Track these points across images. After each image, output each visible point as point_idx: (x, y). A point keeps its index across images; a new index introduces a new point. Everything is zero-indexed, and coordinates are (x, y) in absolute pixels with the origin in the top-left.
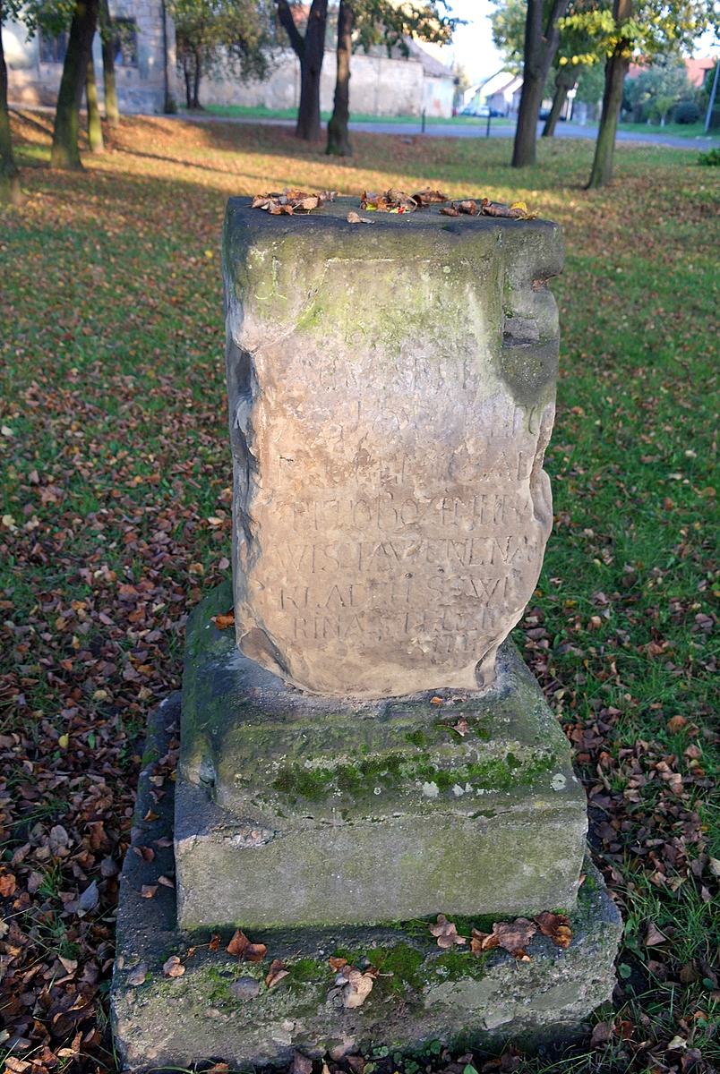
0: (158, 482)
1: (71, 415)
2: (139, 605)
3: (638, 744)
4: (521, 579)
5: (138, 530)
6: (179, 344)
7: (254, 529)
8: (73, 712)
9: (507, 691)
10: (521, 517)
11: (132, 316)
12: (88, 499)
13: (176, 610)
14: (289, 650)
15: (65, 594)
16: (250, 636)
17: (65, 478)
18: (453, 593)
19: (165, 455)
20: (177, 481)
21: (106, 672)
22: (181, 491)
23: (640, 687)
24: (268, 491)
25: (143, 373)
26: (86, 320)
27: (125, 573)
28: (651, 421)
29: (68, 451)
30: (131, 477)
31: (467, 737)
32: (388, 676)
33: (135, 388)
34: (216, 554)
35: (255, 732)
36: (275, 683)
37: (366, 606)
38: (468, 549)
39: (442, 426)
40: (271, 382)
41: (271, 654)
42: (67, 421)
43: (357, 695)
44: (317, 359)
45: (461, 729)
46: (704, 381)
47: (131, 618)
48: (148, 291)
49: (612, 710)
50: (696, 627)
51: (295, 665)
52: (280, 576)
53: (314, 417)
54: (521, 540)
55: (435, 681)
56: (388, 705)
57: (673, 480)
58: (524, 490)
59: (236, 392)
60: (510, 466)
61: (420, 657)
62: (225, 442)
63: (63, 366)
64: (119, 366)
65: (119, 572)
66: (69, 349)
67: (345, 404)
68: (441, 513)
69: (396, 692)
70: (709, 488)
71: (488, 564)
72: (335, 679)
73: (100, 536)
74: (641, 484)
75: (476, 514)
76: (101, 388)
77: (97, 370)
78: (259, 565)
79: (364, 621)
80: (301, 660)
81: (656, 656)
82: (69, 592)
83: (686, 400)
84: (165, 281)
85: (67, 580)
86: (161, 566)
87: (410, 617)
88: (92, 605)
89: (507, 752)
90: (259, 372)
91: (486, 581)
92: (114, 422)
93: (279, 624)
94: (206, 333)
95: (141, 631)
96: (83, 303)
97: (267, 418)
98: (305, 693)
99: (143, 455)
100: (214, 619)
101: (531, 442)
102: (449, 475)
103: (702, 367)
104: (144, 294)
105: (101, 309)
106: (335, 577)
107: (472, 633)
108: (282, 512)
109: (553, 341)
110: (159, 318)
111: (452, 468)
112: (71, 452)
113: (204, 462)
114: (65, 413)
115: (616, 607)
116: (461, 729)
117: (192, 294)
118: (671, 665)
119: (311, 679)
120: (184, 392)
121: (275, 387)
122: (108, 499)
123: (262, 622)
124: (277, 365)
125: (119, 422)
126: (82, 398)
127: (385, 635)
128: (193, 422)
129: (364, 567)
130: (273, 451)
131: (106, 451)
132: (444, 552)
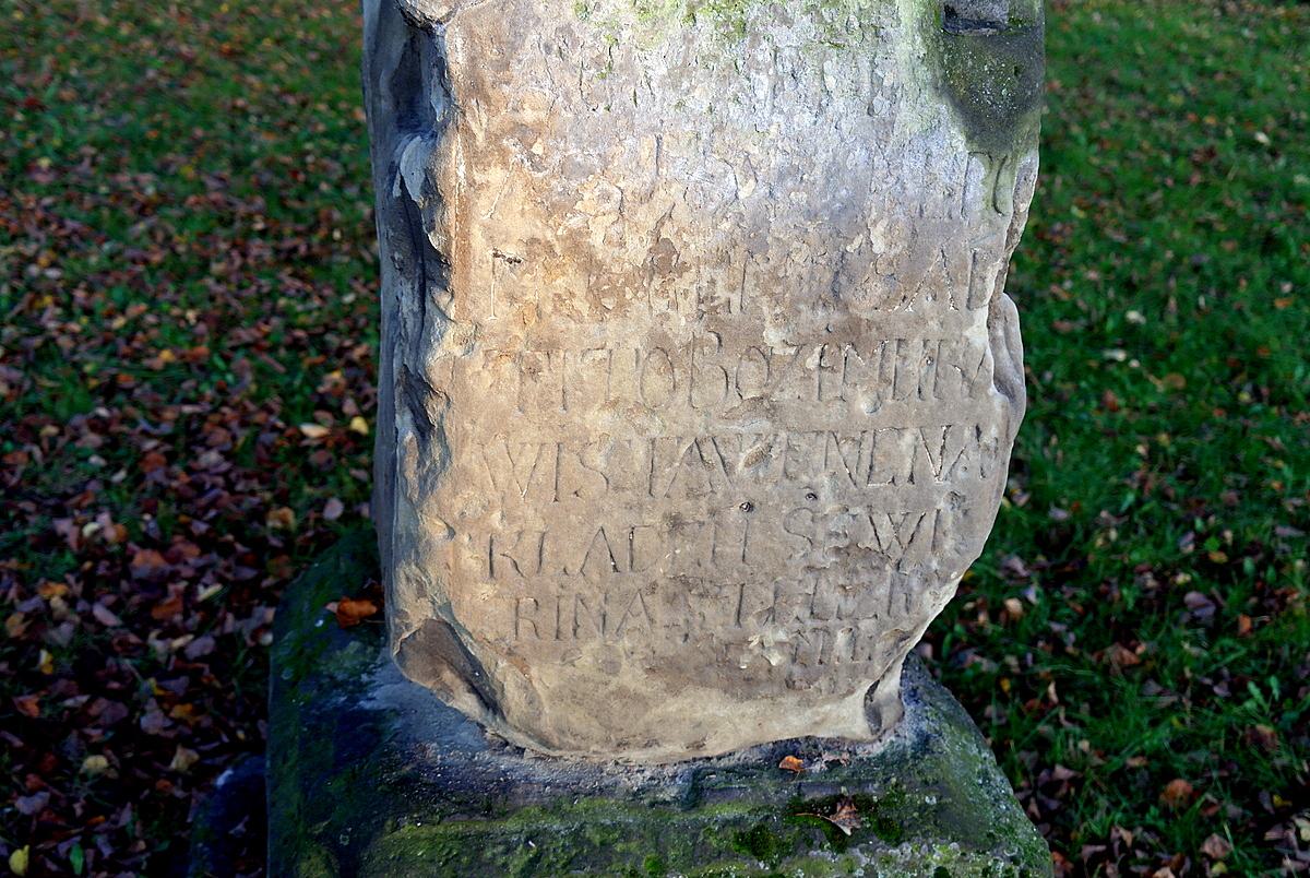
0: (204, 361)
1: (37, 240)
2: (171, 587)
3: (1114, 834)
4: (965, 513)
5: (168, 447)
6: (239, 122)
7: (435, 409)
8: (39, 800)
9: (924, 743)
10: (972, 386)
11: (151, 74)
12: (70, 390)
13: (240, 597)
14: (503, 664)
15: (25, 568)
16: (420, 637)
17: (25, 352)
18: (834, 543)
19: (218, 313)
20: (240, 359)
21: (107, 719)
22: (249, 377)
23: (1106, 727)
24: (468, 328)
25: (172, 169)
26: (66, 78)
27: (143, 527)
28: (1063, 262)
29: (31, 303)
30: (152, 351)
31: (859, 837)
32: (698, 715)
33: (160, 193)
34: (318, 493)
35: (432, 839)
36: (465, 735)
37: (660, 571)
38: (866, 453)
39: (823, 194)
40: (477, 89)
41: (461, 674)
42: (29, 249)
43: (636, 756)
44: (575, 41)
45: (845, 820)
46: (1142, 197)
47: (157, 614)
48: (179, 33)
49: (1061, 772)
50: (1186, 618)
51: (513, 697)
52: (488, 507)
53: (564, 169)
54: (968, 433)
55: (790, 723)
56: (696, 774)
57: (1112, 361)
58: (978, 334)
59: (391, 128)
60: (953, 281)
61: (763, 675)
62: (327, 292)
63: (22, 153)
64: (127, 156)
65: (132, 525)
66: (33, 124)
67: (630, 141)
68: (815, 376)
69: (713, 748)
70: (1174, 376)
71: (903, 483)
72: (595, 723)
73: (94, 459)
74: (1060, 369)
75: (883, 378)
76: (94, 192)
77: (87, 162)
78: (444, 487)
79: (656, 604)
80: (527, 686)
81: (1127, 670)
82: (33, 564)
83: (1117, 227)
84: (210, 17)
85: (30, 542)
86: (212, 513)
87: (747, 592)
88: (78, 589)
89: (934, 866)
90: (454, 68)
91: (898, 517)
92: (119, 253)
93: (484, 610)
94: (285, 105)
95: (175, 637)
96: (59, 48)
97: (469, 167)
98: (528, 754)
99: (176, 311)
100: (333, 607)
101: (997, 230)
102: (834, 297)
103: (1135, 175)
104: (171, 36)
105: (93, 60)
106: (600, 511)
107: (867, 625)
108: (495, 371)
109: (1034, 29)
110: (200, 77)
111: (843, 271)
112: (38, 304)
113: (289, 327)
114: (26, 236)
115: (1044, 583)
116: (845, 820)
117: (259, 39)
118: (1153, 687)
119: (546, 725)
120: (250, 203)
121: (487, 100)
122: (109, 391)
123: (448, 607)
124: (492, 54)
125: (129, 253)
126: (59, 210)
127: (697, 632)
128: (268, 255)
129: (659, 489)
130: (478, 241)
131: (104, 304)
132: (818, 458)
